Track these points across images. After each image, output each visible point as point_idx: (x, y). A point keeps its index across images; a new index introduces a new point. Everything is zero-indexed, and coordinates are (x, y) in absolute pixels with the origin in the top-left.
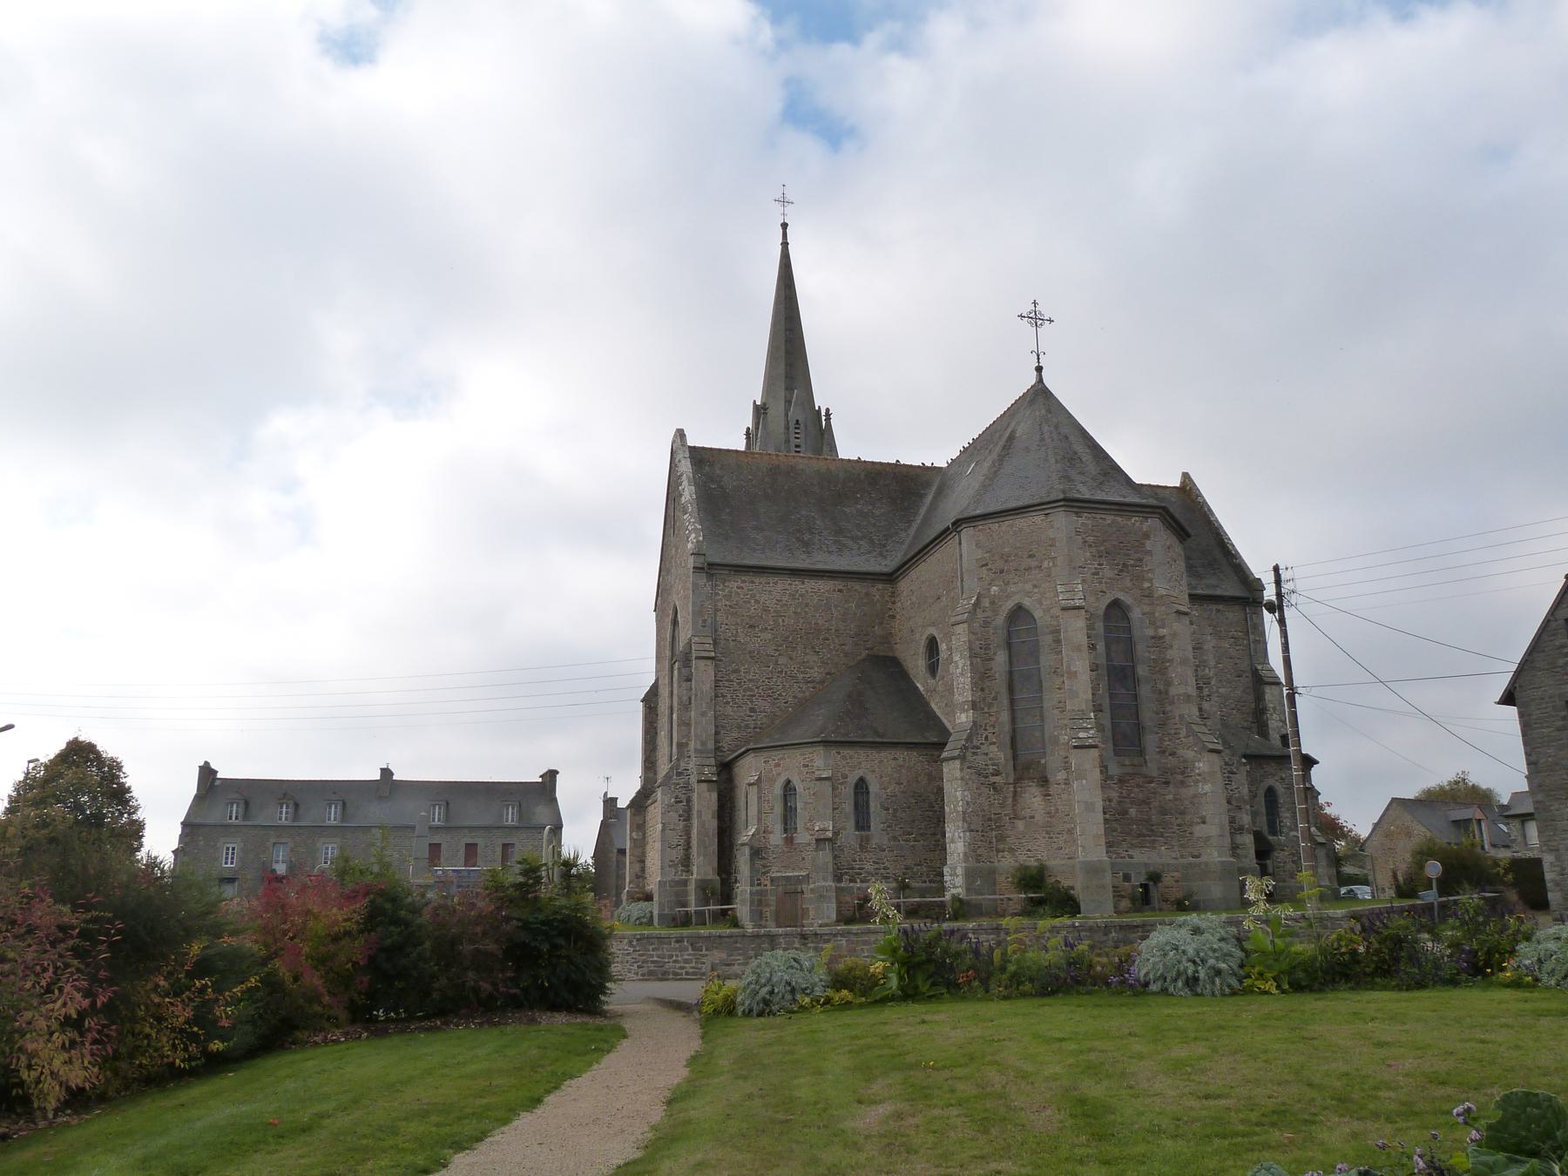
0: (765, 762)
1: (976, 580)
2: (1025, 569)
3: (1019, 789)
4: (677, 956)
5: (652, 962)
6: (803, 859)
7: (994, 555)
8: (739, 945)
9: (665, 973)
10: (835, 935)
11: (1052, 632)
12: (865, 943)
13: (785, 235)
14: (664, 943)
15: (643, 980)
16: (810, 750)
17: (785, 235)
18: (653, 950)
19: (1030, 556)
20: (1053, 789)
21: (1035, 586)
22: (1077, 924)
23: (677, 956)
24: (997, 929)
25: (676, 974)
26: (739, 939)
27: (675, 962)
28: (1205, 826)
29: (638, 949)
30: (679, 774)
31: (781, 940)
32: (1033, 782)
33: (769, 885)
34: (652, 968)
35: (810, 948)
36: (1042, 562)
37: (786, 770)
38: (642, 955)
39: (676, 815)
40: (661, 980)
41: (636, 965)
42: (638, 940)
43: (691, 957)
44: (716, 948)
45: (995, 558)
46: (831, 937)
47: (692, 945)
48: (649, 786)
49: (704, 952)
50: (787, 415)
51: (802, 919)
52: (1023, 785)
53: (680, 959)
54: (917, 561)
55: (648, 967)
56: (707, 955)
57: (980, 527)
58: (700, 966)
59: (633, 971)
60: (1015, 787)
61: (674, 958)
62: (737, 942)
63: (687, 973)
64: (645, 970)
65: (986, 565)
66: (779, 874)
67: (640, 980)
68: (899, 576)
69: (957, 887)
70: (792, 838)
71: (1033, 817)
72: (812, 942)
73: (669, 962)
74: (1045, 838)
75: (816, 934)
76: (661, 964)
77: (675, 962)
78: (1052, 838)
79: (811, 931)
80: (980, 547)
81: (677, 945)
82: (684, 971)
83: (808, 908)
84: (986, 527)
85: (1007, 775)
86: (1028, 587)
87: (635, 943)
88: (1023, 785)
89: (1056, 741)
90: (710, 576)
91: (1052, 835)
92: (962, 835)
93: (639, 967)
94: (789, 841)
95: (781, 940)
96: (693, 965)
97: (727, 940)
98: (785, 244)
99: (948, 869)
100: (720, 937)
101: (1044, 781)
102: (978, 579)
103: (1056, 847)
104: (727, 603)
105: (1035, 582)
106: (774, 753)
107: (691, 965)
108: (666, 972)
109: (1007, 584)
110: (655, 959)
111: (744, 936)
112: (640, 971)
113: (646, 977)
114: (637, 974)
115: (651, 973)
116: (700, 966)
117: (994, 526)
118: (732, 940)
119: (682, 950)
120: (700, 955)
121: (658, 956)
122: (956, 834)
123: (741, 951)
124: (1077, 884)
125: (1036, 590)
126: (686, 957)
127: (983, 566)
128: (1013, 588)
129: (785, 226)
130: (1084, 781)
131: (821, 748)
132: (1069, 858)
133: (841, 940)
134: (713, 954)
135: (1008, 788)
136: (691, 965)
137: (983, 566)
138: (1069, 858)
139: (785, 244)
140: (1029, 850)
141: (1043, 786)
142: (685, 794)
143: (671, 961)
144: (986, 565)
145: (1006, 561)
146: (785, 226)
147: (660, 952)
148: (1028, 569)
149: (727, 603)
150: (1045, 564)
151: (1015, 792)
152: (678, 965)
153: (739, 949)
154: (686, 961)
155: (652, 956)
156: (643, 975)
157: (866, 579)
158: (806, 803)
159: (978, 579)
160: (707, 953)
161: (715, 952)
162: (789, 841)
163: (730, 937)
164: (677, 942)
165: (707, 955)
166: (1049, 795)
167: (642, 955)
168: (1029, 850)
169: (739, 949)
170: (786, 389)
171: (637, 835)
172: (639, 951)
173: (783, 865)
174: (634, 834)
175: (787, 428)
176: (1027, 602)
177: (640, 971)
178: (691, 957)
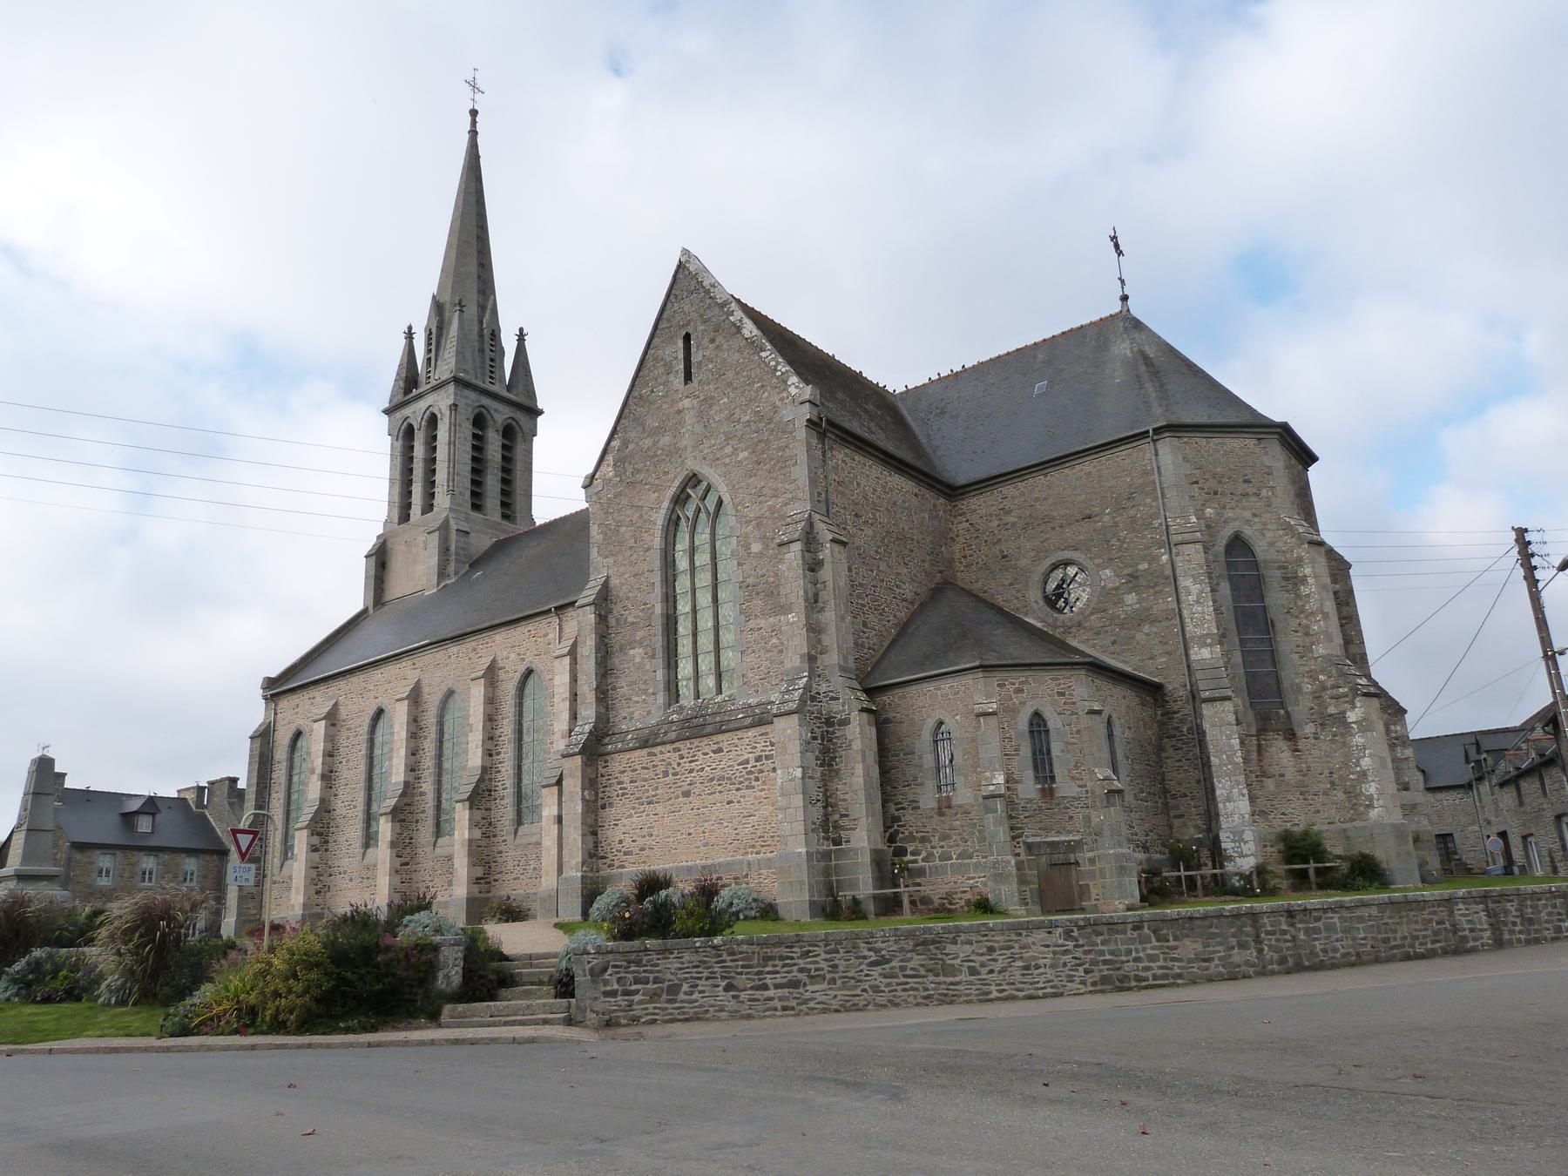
0: (999, 685)
1: (1187, 497)
2: (1241, 494)
3: (1263, 742)
4: (1137, 951)
5: (1105, 962)
6: (1071, 818)
7: (1204, 474)
8: (1213, 930)
9: (1126, 978)
10: (1325, 911)
11: (1280, 568)
12: (1361, 919)
13: (474, 123)
14: (1117, 932)
15: (1096, 992)
16: (1068, 673)
17: (474, 123)
18: (1102, 944)
19: (1246, 481)
20: (1301, 744)
21: (1255, 515)
22: (1553, 889)
23: (1137, 951)
24: (1485, 897)
25: (1138, 979)
26: (1215, 921)
27: (1137, 960)
28: (1408, 792)
29: (1081, 942)
30: (813, 699)
31: (1266, 921)
32: (1278, 734)
33: (1023, 854)
34: (1106, 973)
35: (1300, 929)
36: (1259, 489)
37: (1033, 698)
38: (1088, 952)
39: (813, 757)
40: (1121, 989)
41: (1081, 969)
42: (1080, 928)
43: (1155, 952)
44: (1187, 936)
45: (1207, 477)
46: (1321, 913)
47: (1154, 932)
48: (602, 726)
49: (1172, 943)
50: (481, 322)
51: (1081, 899)
52: (1268, 738)
53: (1141, 955)
54: (1014, 477)
55: (1101, 971)
56: (1175, 948)
57: (1185, 440)
58: (1170, 964)
59: (1077, 980)
60: (1258, 740)
61: (1134, 954)
62: (1211, 927)
63: (1155, 977)
64: (1096, 976)
65: (1197, 482)
66: (1038, 839)
67: (1091, 992)
68: (969, 492)
69: (1247, 856)
70: (1051, 789)
71: (1283, 775)
72: (1301, 922)
73: (1128, 961)
74: (1298, 799)
75: (1305, 910)
76: (1118, 965)
77: (1137, 960)
78: (1307, 799)
79: (1300, 905)
80: (1187, 461)
81: (1135, 934)
82: (1149, 974)
83: (1088, 885)
84: (1193, 440)
85: (1249, 725)
86: (1247, 514)
87: (1075, 934)
88: (1268, 738)
89: (1299, 689)
90: (822, 436)
91: (1307, 797)
92: (1245, 791)
93: (1086, 972)
94: (1048, 793)
95: (1266, 921)
96: (1161, 963)
97: (1199, 922)
98: (474, 133)
99: (1228, 834)
100: (1191, 918)
101: (1291, 735)
102: (1190, 497)
103: (1313, 810)
104: (836, 478)
105: (1254, 510)
106: (1014, 674)
107: (1158, 964)
108: (1126, 976)
109: (1224, 507)
110: (1108, 957)
111: (1221, 916)
112: (1090, 979)
113: (1099, 988)
114: (1083, 983)
115: (1105, 980)
116: (1170, 964)
117: (1200, 441)
118: (1207, 922)
119: (1144, 940)
120: (1168, 948)
121: (1112, 953)
122: (1235, 790)
123: (1219, 939)
124: (1385, 853)
125: (1257, 519)
126: (1151, 952)
127: (1193, 483)
128: (1229, 514)
129: (474, 113)
130: (1375, 733)
131: (1084, 672)
132: (1329, 823)
133: (1332, 918)
134: (1185, 945)
135: (1251, 741)
136: (1158, 964)
137: (1193, 483)
138: (1329, 823)
139: (474, 133)
140: (1283, 814)
141: (1290, 740)
142: (819, 728)
143: (1130, 958)
144: (1197, 482)
145: (1220, 482)
146: (474, 113)
147: (1112, 947)
148: (1245, 495)
149: (836, 478)
150: (1264, 493)
151: (1259, 746)
152: (1141, 965)
153: (1215, 935)
154: (1152, 958)
155: (1102, 953)
156: (1094, 984)
157: (934, 487)
158: (1068, 743)
159: (1190, 497)
160: (1176, 943)
161: (1187, 942)
162: (1048, 793)
163: (1205, 917)
164: (1135, 928)
165: (1175, 948)
166: (1299, 751)
167: (1088, 952)
168: (1283, 814)
169: (1215, 935)
170: (479, 292)
171: (589, 794)
172: (1083, 946)
173: (1042, 825)
174: (586, 792)
175: (481, 336)
176: (1248, 532)
177: (1090, 979)
178: (1155, 952)
